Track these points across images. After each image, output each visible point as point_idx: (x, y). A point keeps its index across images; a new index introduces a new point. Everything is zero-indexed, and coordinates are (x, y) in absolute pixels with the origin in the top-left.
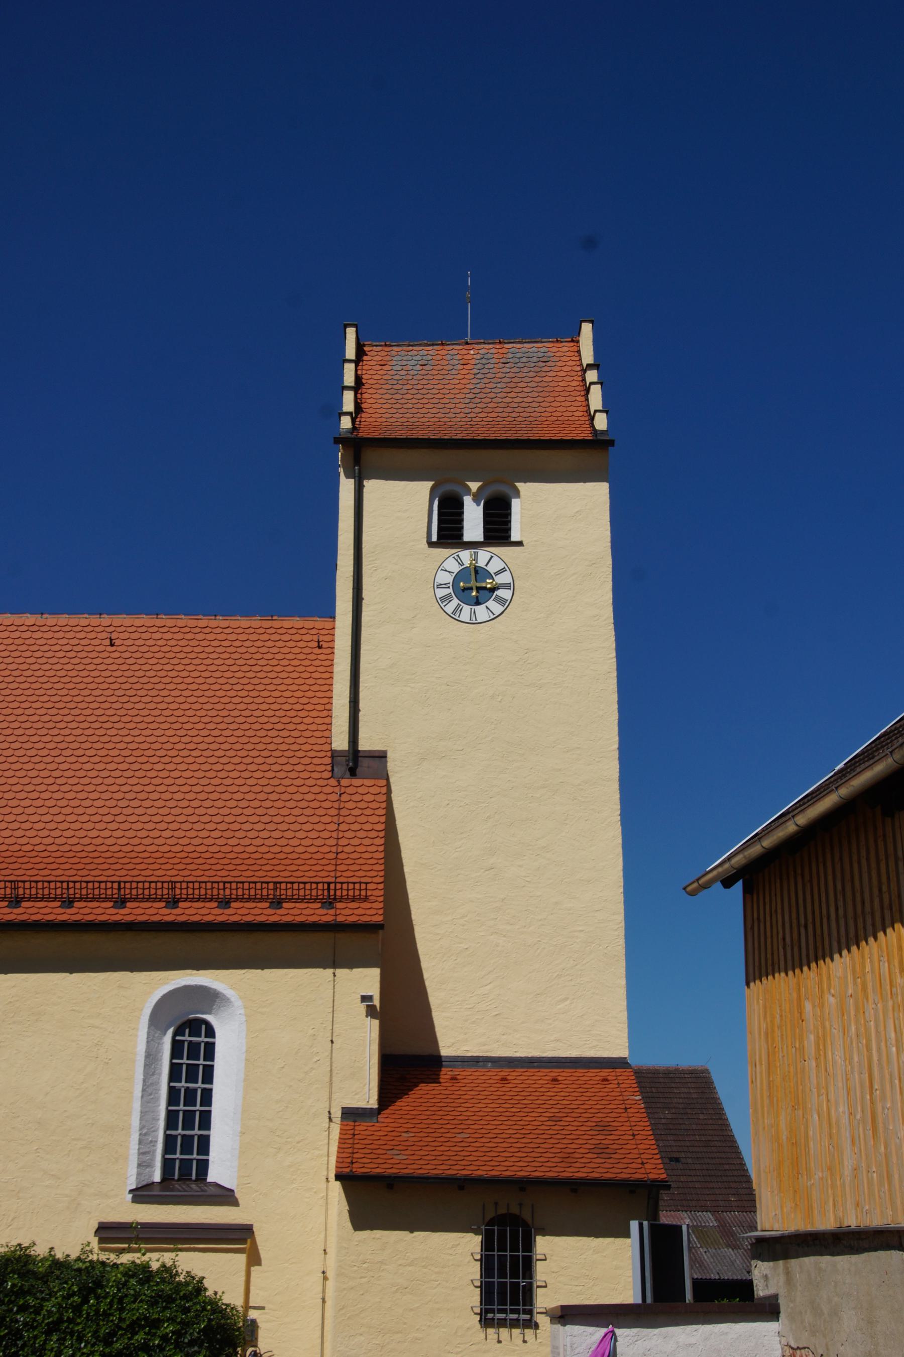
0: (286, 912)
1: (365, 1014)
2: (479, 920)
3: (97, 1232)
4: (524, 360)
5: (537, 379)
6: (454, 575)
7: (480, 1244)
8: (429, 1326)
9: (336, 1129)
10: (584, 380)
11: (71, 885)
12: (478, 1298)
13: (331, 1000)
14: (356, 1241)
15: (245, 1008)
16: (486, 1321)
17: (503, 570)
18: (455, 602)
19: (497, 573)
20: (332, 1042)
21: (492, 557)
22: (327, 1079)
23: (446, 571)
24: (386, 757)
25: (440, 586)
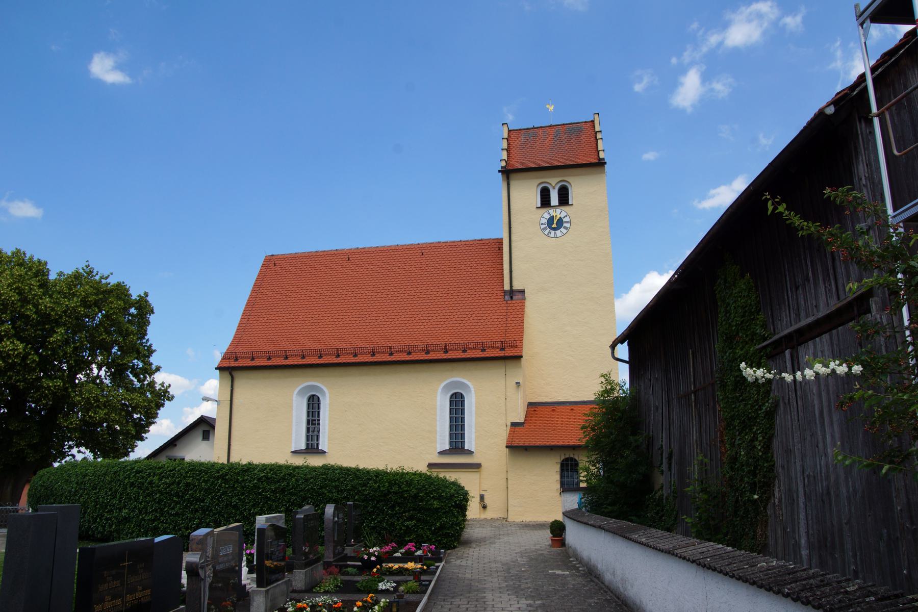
0: (468, 354)
1: (216, 367)
3: (428, 466)
4: (573, 131)
5: (578, 139)
10: (596, 137)
11: (410, 347)
15: (474, 388)
17: (566, 216)
18: (565, 225)
22: (505, 412)
24: (524, 291)
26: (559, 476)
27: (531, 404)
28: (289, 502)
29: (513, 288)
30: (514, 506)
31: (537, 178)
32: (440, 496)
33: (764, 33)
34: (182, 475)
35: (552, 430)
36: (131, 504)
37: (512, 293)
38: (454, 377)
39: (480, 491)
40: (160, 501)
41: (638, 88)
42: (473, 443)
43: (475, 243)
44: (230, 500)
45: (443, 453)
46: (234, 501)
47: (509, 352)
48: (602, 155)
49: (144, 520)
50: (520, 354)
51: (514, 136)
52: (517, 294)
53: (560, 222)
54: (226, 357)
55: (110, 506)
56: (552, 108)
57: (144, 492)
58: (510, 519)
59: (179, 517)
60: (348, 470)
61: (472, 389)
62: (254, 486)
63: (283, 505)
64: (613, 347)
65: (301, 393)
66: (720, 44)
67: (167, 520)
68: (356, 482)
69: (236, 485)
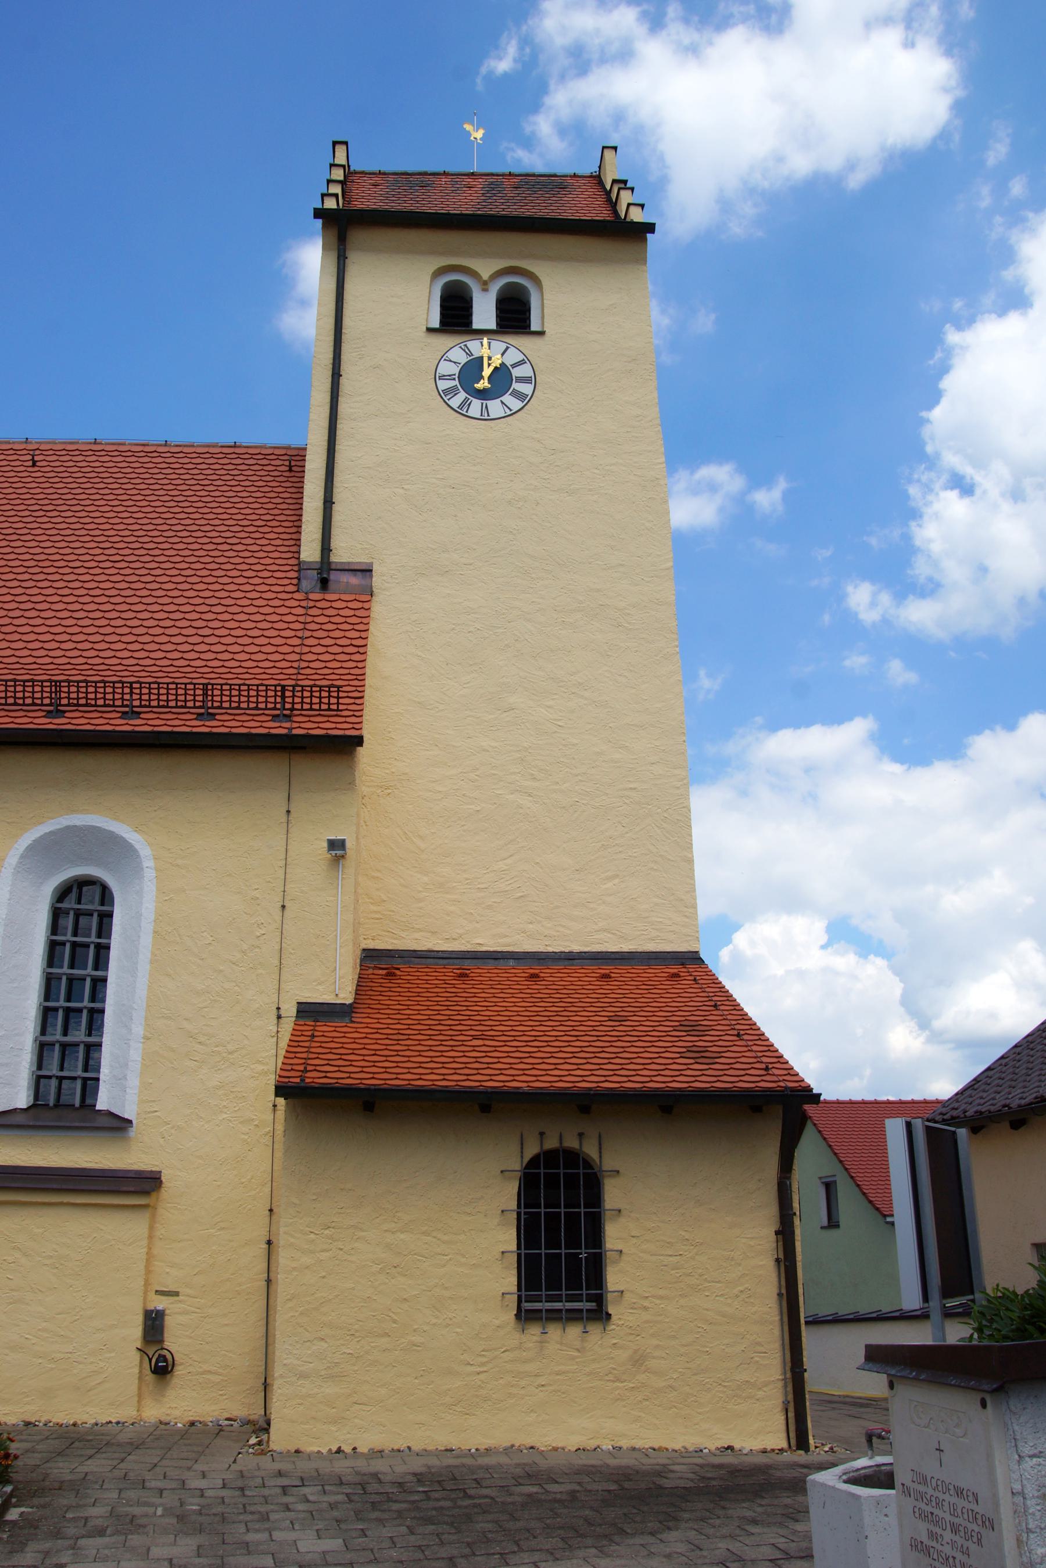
2: (494, 774)
6: (460, 366)
7: (516, 1198)
8: (434, 1324)
9: (288, 1026)
12: (514, 1280)
13: (284, 850)
14: (314, 1194)
16: (525, 1316)
17: (521, 363)
18: (516, 386)
19: (514, 366)
20: (283, 907)
21: (507, 348)
23: (450, 361)
27: (370, 957)
29: (336, 558)
30: (303, 1376)
31: (433, 252)
33: (721, 510)
35: (475, 1038)
38: (74, 812)
39: (145, 1293)
42: (133, 1082)
45: (115, 1123)
53: (502, 377)
56: (479, 134)
58: (280, 1439)
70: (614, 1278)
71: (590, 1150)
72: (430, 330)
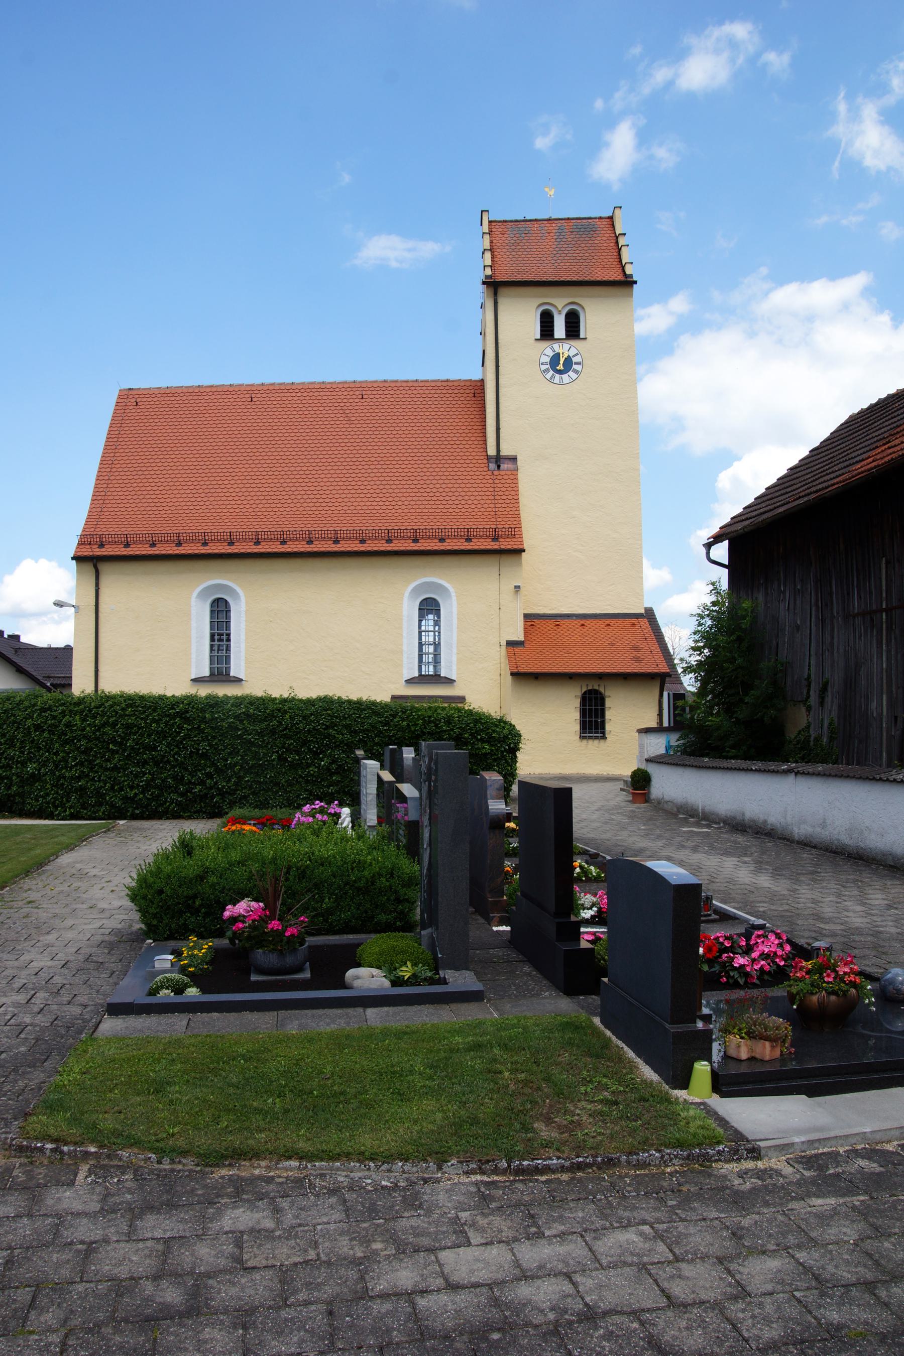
16: (582, 738)
17: (577, 354)
18: (574, 367)
19: (574, 356)
25: (543, 364)
26: (578, 714)
28: (283, 747)
29: (502, 454)
32: (491, 737)
34: (117, 713)
36: (41, 756)
37: (498, 459)
40: (87, 751)
41: (541, 143)
42: (454, 667)
43: (439, 384)
44: (196, 746)
46: (204, 747)
47: (505, 544)
48: (629, 270)
49: (64, 778)
50: (521, 547)
51: (497, 229)
52: (507, 461)
53: (569, 362)
54: (83, 542)
55: (6, 758)
56: (552, 193)
57: (59, 738)
59: (119, 773)
60: (359, 703)
61: (453, 594)
62: (230, 726)
63: (274, 752)
64: (708, 546)
65: (202, 595)
66: (670, 84)
67: (100, 776)
68: (375, 719)
69: (203, 726)
70: (608, 727)
71: (602, 690)
72: (536, 340)
